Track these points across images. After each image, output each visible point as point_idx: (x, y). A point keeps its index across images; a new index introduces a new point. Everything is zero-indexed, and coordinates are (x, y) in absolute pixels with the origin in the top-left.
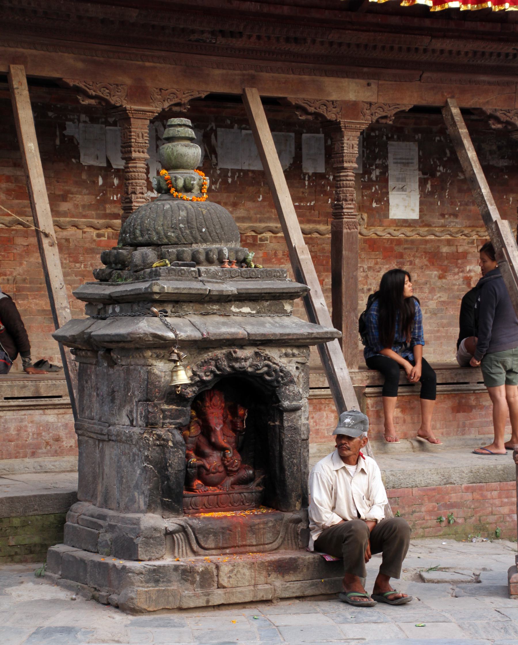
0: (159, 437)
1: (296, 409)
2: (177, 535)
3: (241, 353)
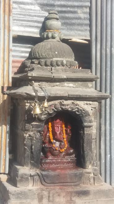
0: (30, 136)
1: (90, 127)
2: (35, 177)
3: (65, 102)
